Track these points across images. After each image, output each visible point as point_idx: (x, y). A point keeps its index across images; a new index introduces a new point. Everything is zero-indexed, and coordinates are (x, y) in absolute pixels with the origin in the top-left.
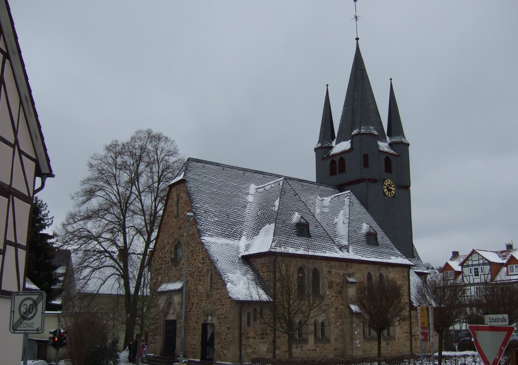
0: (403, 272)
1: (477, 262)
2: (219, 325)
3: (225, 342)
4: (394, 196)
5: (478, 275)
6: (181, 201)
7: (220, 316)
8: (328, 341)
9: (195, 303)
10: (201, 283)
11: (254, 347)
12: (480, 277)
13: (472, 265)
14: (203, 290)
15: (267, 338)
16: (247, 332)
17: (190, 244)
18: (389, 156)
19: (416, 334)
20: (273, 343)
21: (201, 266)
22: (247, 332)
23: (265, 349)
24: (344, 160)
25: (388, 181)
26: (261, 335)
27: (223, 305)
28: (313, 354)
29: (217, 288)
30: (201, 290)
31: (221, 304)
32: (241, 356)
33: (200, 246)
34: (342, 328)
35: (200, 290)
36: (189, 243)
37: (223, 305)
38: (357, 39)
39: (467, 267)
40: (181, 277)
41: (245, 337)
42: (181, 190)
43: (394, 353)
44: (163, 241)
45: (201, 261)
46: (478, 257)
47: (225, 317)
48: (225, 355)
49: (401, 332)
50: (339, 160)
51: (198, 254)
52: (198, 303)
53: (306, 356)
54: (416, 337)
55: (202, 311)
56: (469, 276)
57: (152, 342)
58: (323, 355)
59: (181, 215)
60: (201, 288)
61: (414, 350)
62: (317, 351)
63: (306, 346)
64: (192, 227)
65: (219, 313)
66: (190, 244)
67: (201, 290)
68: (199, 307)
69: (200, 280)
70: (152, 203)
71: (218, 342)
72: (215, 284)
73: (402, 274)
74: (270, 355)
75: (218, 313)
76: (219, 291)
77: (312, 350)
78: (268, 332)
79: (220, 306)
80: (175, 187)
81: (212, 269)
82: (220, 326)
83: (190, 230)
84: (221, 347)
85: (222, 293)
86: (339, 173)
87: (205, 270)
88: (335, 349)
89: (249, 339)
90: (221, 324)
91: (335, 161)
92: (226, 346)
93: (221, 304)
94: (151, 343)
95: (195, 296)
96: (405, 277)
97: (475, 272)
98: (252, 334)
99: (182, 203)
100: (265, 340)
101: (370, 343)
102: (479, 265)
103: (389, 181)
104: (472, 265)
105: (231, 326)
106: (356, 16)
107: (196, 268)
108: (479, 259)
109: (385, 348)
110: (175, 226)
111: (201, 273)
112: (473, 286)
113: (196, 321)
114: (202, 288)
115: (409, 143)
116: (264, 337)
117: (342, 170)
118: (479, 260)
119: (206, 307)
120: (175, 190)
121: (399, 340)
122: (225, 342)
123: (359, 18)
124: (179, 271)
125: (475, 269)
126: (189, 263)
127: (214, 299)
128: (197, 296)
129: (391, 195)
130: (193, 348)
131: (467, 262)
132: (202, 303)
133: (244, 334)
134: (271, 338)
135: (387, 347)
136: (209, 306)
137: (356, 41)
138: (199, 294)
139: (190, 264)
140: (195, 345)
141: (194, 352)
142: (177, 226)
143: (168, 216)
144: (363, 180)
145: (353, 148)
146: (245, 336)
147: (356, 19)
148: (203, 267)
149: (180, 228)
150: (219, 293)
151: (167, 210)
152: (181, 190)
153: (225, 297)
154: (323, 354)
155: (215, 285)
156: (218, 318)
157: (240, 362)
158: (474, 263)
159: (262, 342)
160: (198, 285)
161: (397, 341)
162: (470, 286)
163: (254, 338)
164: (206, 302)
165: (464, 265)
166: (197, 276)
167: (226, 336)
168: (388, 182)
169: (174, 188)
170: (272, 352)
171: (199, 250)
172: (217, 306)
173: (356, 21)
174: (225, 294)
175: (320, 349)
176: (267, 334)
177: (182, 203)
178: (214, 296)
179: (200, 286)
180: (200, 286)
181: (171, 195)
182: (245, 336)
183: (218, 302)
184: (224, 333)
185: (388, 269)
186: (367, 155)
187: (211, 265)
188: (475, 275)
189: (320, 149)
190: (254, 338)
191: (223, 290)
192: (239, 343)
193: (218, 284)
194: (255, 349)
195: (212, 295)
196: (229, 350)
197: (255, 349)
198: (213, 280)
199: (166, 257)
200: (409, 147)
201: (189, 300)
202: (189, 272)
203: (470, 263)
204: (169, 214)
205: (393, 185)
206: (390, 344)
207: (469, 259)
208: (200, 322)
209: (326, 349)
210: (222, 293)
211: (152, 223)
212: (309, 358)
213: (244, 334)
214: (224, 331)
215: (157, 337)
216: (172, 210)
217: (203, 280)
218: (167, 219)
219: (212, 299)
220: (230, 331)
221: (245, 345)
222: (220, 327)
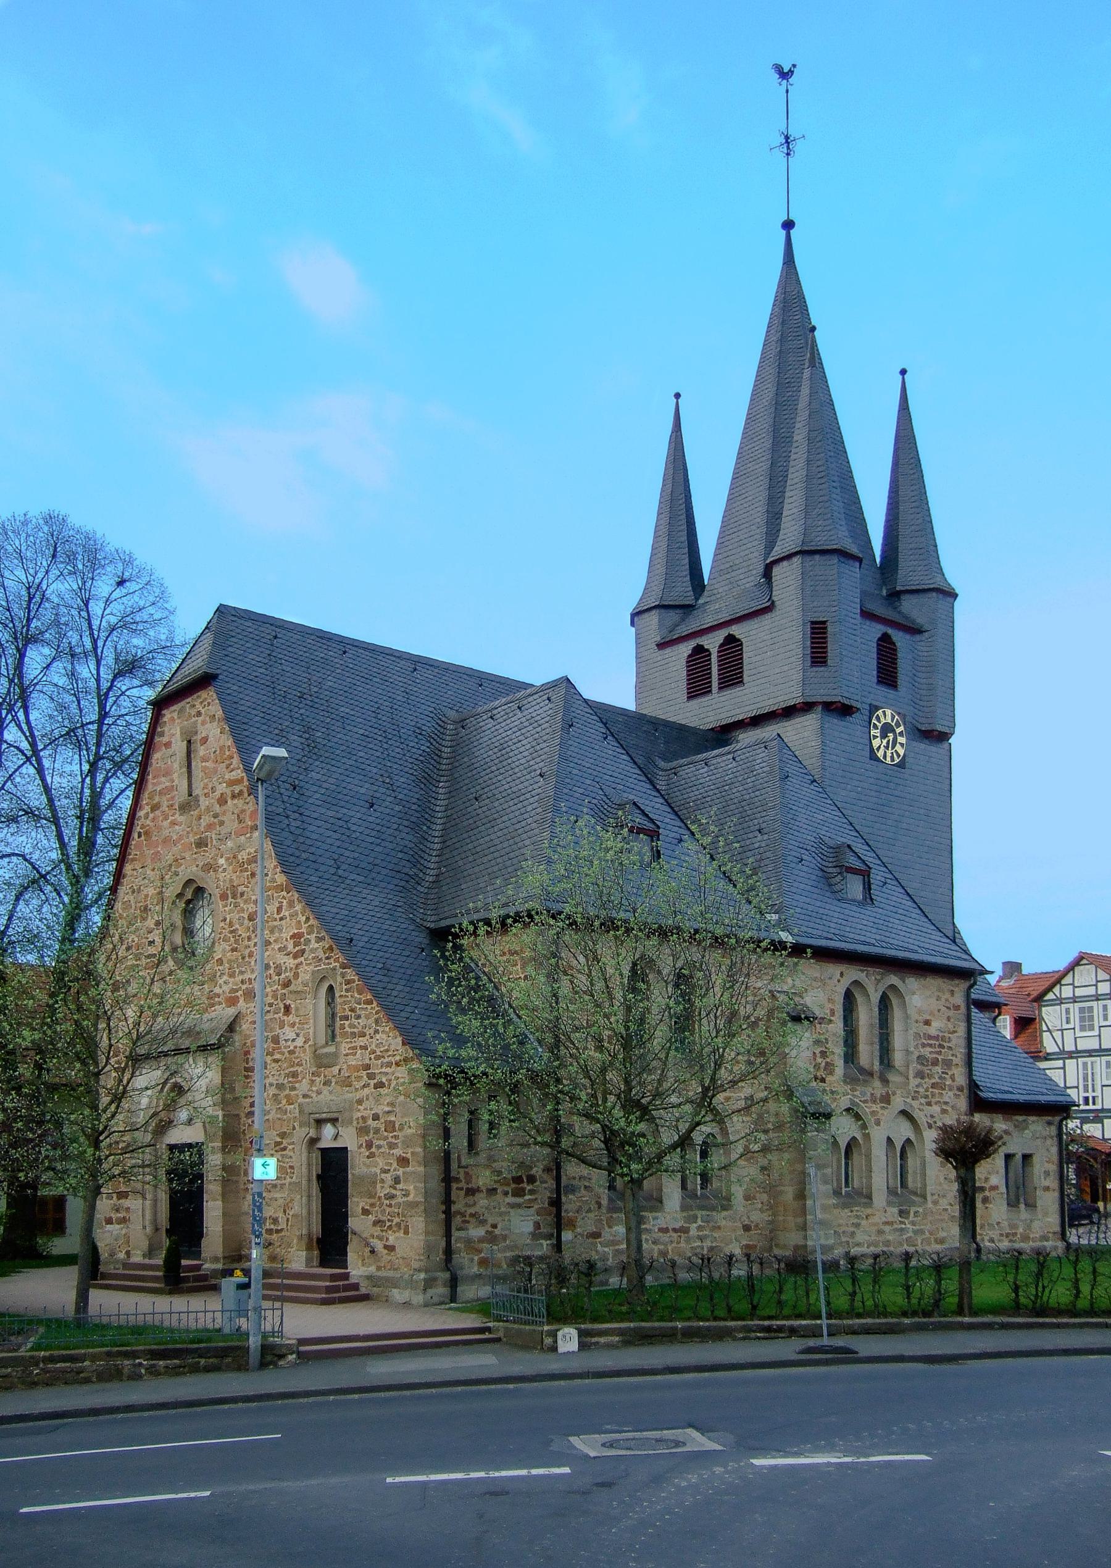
0: (952, 993)
1: (1091, 991)
2: (367, 1154)
3: (390, 1206)
4: (902, 765)
5: (1092, 1028)
6: (201, 751)
7: (370, 1122)
8: (725, 1203)
9: (271, 1085)
10: (291, 1018)
11: (491, 1221)
12: (1097, 1034)
13: (1074, 1000)
14: (300, 1042)
15: (532, 1192)
16: (467, 1174)
17: (242, 894)
18: (890, 631)
19: (987, 1186)
20: (554, 1209)
21: (291, 962)
22: (467, 1174)
23: (529, 1227)
24: (741, 645)
25: (884, 713)
26: (514, 1182)
27: (380, 1085)
28: (678, 1243)
29: (352, 1033)
30: (293, 1040)
31: (372, 1082)
32: (448, 1252)
33: (284, 897)
34: (765, 1162)
35: (289, 1043)
36: (241, 889)
37: (380, 1085)
38: (788, 225)
39: (1057, 1004)
40: (213, 1005)
41: (462, 1189)
42: (199, 714)
43: (923, 1240)
44: (139, 891)
45: (290, 947)
46: (1094, 976)
47: (390, 1126)
48: (391, 1248)
49: (942, 1179)
50: (721, 645)
51: (275, 923)
52: (280, 1087)
53: (656, 1248)
54: (987, 1193)
55: (297, 1111)
56: (1062, 1030)
57: (111, 1218)
58: (709, 1244)
59: (202, 799)
60: (293, 1036)
61: (981, 1235)
62: (691, 1233)
63: (655, 1218)
64: (251, 837)
65: (365, 1113)
66: (242, 894)
67: (293, 1040)
68: (287, 1097)
69: (287, 1009)
70: (83, 781)
71: (363, 1208)
72: (346, 1018)
73: (947, 1000)
74: (545, 1246)
75: (359, 1115)
76: (362, 1041)
77: (675, 1230)
78: (537, 1171)
79: (366, 1091)
80: (176, 707)
81: (334, 969)
82: (371, 1156)
83: (240, 848)
84: (376, 1223)
85: (373, 1047)
86: (722, 687)
87: (308, 977)
88: (747, 1228)
89: (473, 1195)
90: (373, 1150)
91: (708, 650)
92: (396, 1220)
93: (372, 1082)
94: (109, 1221)
95: (269, 1062)
96: (957, 1008)
97: (1082, 1019)
98: (483, 1178)
99: (204, 759)
100: (527, 1197)
101: (852, 1211)
102: (1097, 998)
103: (889, 712)
104: (1074, 1000)
105: (412, 1153)
106: (787, 138)
107: (271, 971)
108: (1098, 981)
109: (895, 1226)
110: (181, 838)
111: (292, 988)
112: (1072, 1058)
113: (277, 1144)
114: (298, 1035)
115: (957, 591)
116: (523, 1189)
117: (732, 677)
118: (1096, 985)
119: (314, 1095)
120: (175, 715)
121: (935, 1203)
122: (390, 1206)
123: (798, 147)
124: (206, 986)
125: (1082, 1010)
126: (243, 958)
127: (345, 1067)
128: (276, 1061)
129: (892, 759)
130: (270, 1232)
131: (1056, 990)
132: (297, 1085)
133: (457, 1180)
134: (545, 1189)
135: (901, 1222)
136: (325, 1092)
137: (784, 233)
138: (287, 1054)
139: (247, 959)
140: (275, 1221)
141: (270, 1244)
142: (192, 839)
143: (155, 808)
144: (807, 707)
145: (773, 602)
146: (463, 1184)
147: (788, 148)
148: (298, 966)
149: (201, 844)
150: (365, 1048)
151: (150, 787)
152: (199, 714)
153: (387, 1060)
154: (708, 1243)
155: (347, 1023)
156: (363, 1130)
157: (448, 1269)
158: (1079, 992)
159: (519, 1206)
160: (282, 1027)
161: (930, 1205)
162: (1064, 1059)
163: (492, 1191)
164: (313, 1081)
165: (1046, 998)
166: (275, 997)
167: (395, 1189)
168: (887, 716)
169: (172, 708)
170: (549, 1236)
171: (279, 910)
172: (357, 1090)
173: (788, 154)
174: (387, 1051)
175: (699, 1228)
176: (531, 1179)
177: (204, 759)
178: (342, 1059)
179: (287, 1029)
180: (287, 1029)
181: (162, 734)
182: (460, 1185)
183: (359, 1078)
184: (388, 1177)
185: (907, 981)
186: (824, 622)
187: (327, 958)
188: (1083, 1029)
189: (654, 612)
190: (492, 1191)
191: (378, 1037)
192: (443, 1207)
193: (359, 1017)
194: (495, 1226)
195: (335, 1055)
196: (406, 1232)
197: (495, 1226)
198: (339, 1007)
199: (151, 943)
200: (956, 603)
201: (247, 1077)
202: (244, 987)
203: (1067, 992)
204: (157, 799)
205: (902, 728)
206: (909, 1213)
207: (1063, 982)
208: (290, 1147)
209: (719, 1228)
210: (373, 1047)
211: (87, 847)
212: (664, 1254)
213: (457, 1180)
214: (387, 1171)
215: (133, 1203)
216: (168, 784)
217: (297, 1009)
218: (151, 816)
219: (335, 1070)
220: (409, 1169)
221: (463, 1215)
222: (368, 1157)
